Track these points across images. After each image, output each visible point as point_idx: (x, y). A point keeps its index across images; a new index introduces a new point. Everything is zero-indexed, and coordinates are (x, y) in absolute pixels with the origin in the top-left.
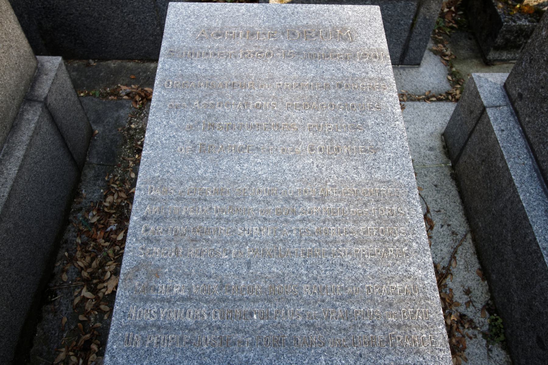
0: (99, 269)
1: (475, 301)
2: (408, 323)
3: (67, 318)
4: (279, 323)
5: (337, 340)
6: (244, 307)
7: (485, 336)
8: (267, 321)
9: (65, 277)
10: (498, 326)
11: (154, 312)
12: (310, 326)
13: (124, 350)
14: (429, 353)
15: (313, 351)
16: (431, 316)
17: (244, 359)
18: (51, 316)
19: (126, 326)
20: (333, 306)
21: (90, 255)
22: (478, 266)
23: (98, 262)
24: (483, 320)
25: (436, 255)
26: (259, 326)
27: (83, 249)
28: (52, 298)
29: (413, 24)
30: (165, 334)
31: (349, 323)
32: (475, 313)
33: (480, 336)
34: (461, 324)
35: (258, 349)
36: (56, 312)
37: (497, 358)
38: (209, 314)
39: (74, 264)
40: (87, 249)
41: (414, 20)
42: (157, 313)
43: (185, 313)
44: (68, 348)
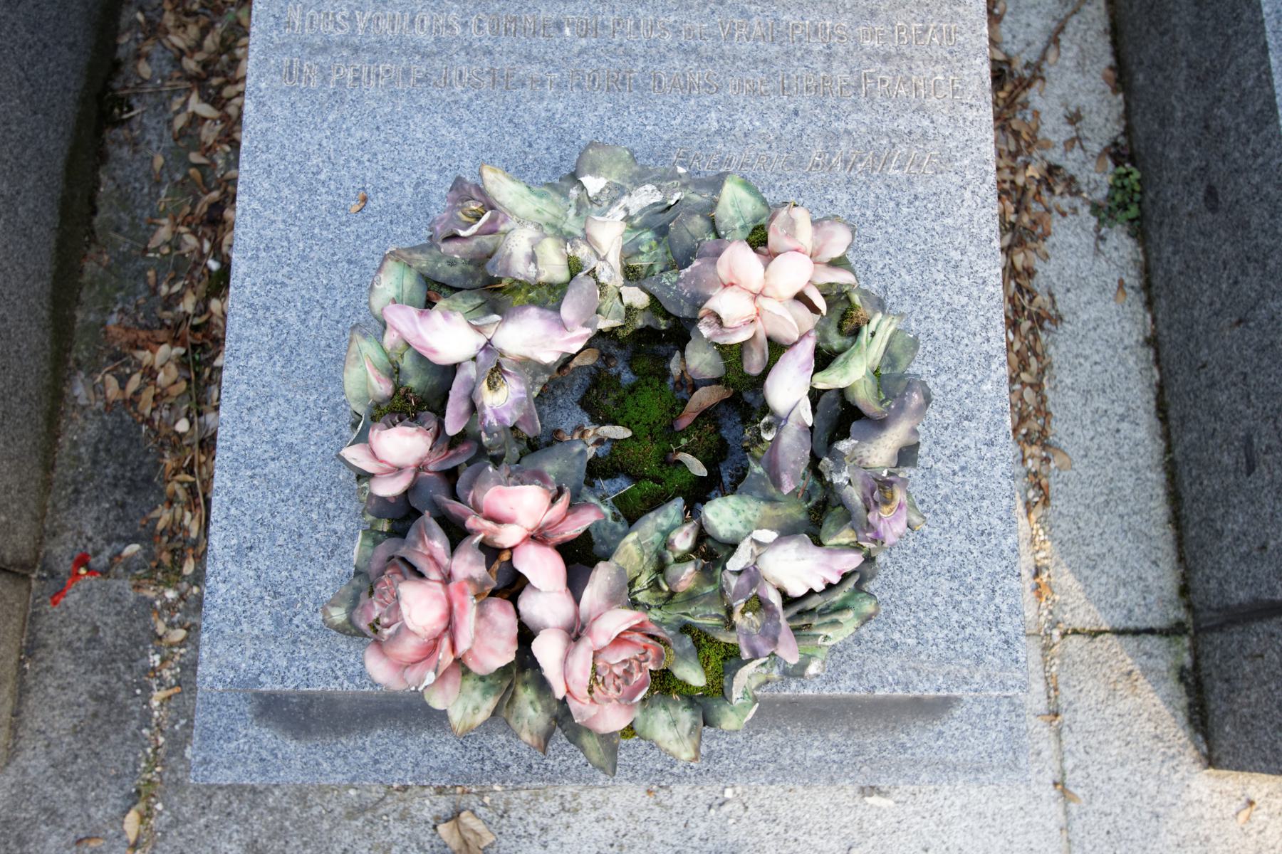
0: (220, 54)
1: (1087, 139)
2: (907, 52)
3: (165, 158)
4: (621, 45)
5: (748, 82)
6: (543, 11)
7: (1096, 208)
8: (594, 40)
9: (145, 69)
10: (1128, 189)
11: (343, 17)
12: (686, 52)
13: (283, 92)
14: (945, 111)
15: (692, 102)
16: (961, 39)
17: (543, 114)
18: (125, 152)
19: (284, 44)
20: (743, 13)
21: (197, 22)
22: (1109, 60)
23: (218, 39)
24: (1098, 177)
25: (1014, 37)
26: (576, 50)
27: (177, 6)
28: (122, 113)
30: (370, 62)
31: (777, 48)
32: (1084, 163)
33: (1085, 211)
34: (1048, 184)
35: (573, 96)
36: (136, 144)
37: (1115, 255)
38: (465, 25)
39: (160, 42)
40: (188, 6)
42: (349, 20)
43: (412, 22)
44: (175, 219)
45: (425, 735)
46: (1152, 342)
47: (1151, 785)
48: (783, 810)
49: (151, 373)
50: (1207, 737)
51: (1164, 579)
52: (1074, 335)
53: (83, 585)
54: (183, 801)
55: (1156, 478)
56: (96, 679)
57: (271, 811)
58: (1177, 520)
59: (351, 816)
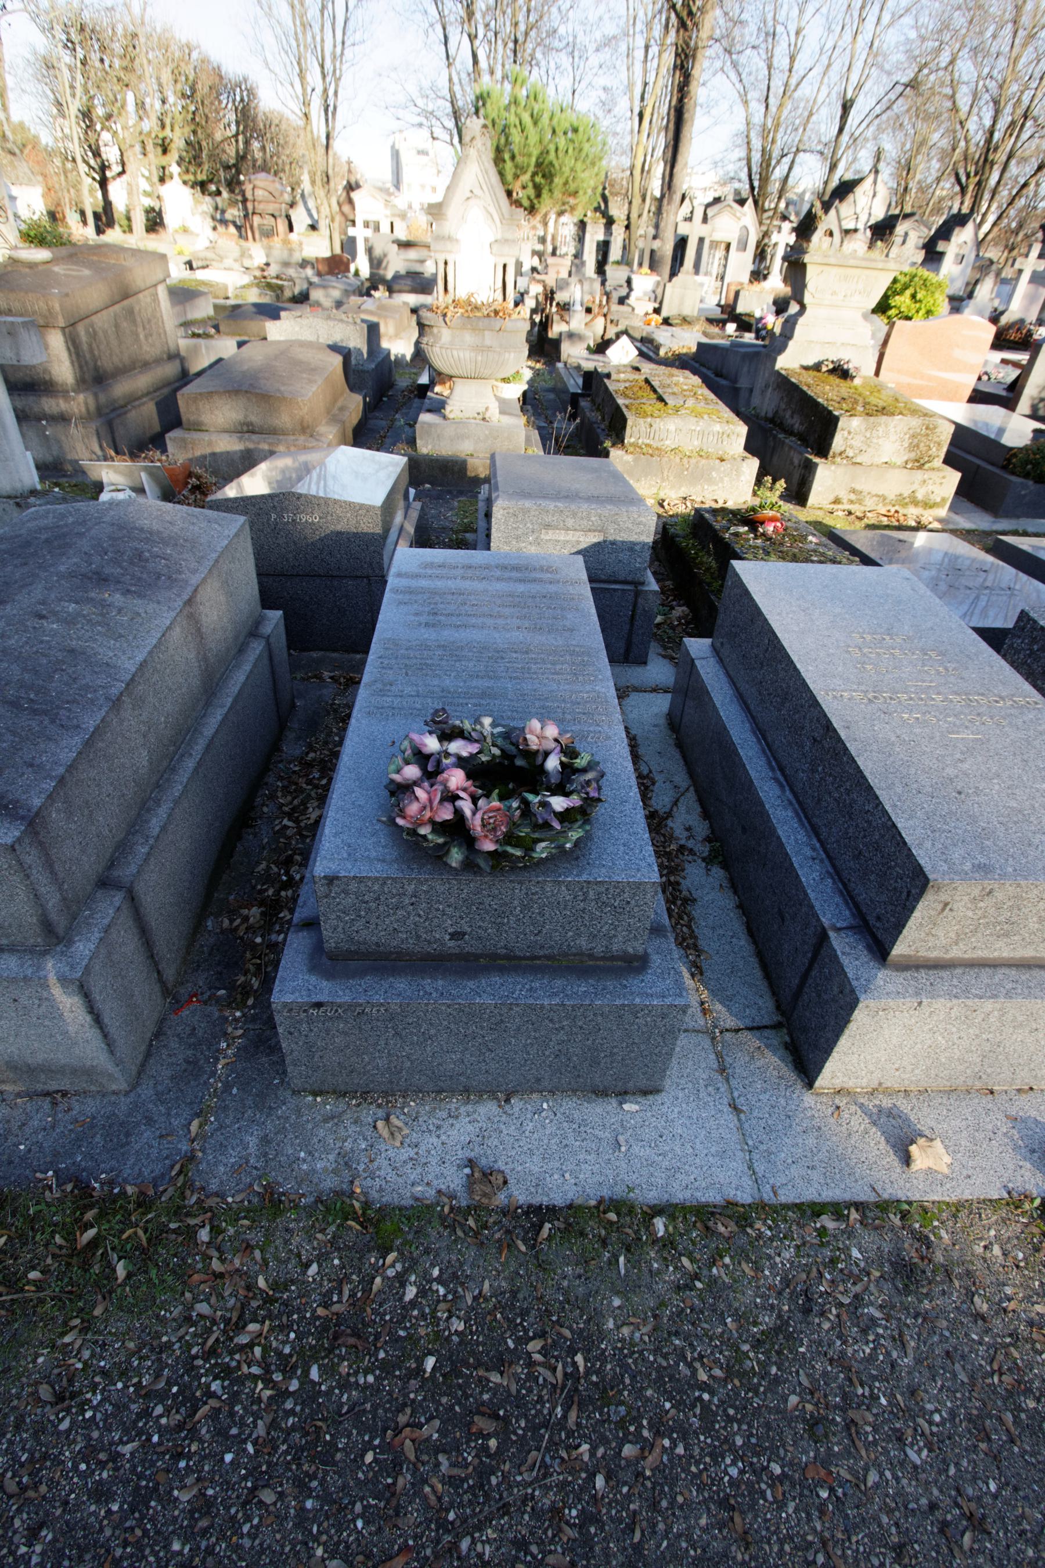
7: (704, 859)
22: (700, 809)
29: (633, 616)
41: (633, 611)
45: (391, 979)
46: (740, 906)
47: (782, 1101)
48: (576, 1115)
49: (246, 919)
50: (807, 1077)
51: (767, 1003)
52: (703, 906)
53: (192, 1007)
54: (227, 1117)
55: (753, 961)
56: (189, 1052)
57: (279, 1118)
58: (767, 976)
59: (326, 1120)
